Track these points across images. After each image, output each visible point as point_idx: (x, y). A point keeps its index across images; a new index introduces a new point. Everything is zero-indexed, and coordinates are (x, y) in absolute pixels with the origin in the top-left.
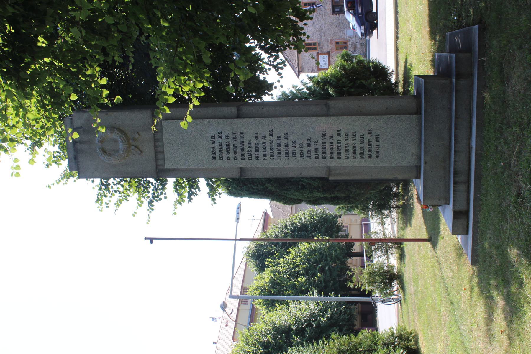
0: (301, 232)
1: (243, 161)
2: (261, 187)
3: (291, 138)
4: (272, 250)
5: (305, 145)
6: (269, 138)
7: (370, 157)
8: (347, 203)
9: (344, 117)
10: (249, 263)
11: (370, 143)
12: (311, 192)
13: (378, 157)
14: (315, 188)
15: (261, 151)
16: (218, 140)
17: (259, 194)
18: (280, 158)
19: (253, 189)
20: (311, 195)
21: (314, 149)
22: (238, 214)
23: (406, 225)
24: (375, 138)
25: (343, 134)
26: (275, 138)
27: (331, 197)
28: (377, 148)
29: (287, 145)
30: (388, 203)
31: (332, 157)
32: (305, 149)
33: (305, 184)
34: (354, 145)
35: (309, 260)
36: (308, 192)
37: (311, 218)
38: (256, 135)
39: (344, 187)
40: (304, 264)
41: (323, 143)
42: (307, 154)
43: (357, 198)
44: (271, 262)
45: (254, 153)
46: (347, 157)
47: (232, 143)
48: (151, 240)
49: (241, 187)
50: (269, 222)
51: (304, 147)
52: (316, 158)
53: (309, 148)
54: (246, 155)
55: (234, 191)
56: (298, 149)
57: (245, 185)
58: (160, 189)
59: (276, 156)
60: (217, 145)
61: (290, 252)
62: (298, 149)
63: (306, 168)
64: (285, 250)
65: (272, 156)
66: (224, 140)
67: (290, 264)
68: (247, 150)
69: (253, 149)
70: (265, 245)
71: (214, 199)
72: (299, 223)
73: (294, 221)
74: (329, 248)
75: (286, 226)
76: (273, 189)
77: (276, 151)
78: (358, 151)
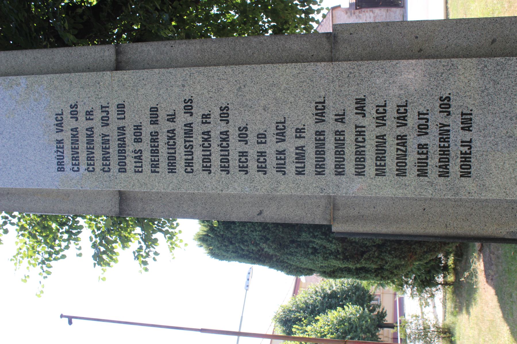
0: (331, 301)
1: (123, 175)
2: (254, 248)
3: (237, 120)
4: (300, 316)
5: (271, 139)
6: (182, 119)
7: (444, 173)
8: (379, 278)
9: (374, 62)
10: (277, 328)
11: (444, 133)
12: (326, 259)
13: (466, 173)
14: (331, 253)
15: (163, 151)
16: (69, 123)
17: (250, 258)
18: (207, 169)
19: (243, 250)
20: (325, 264)
21: (293, 149)
22: (248, 280)
23: (461, 310)
24: (459, 120)
25: (370, 110)
26: (196, 120)
27: (357, 269)
28: (465, 149)
29: (225, 136)
30: (434, 277)
31: (340, 171)
32: (271, 147)
33: (317, 247)
34: (402, 140)
35: (337, 330)
36: (321, 258)
37: (342, 285)
38: (154, 111)
39: (376, 254)
40: (332, 334)
41: (319, 133)
42: (275, 162)
43: (395, 271)
44: (298, 329)
45: (147, 156)
46: (380, 172)
47: (99, 130)
48: (70, 319)
49: (226, 246)
50: (300, 286)
51: (269, 144)
52: (299, 173)
53: (281, 146)
54: (130, 162)
55: (217, 251)
56: (253, 149)
57: (231, 243)
58: (64, 241)
59: (198, 165)
60: (66, 136)
61: (318, 320)
62: (253, 149)
63: (273, 199)
64: (314, 317)
65: (189, 163)
66: (82, 124)
67: (318, 333)
68: (131, 148)
69: (145, 146)
70: (293, 311)
71: (145, 263)
72: (330, 289)
73: (325, 287)
74: (359, 318)
75: (316, 292)
76: (271, 252)
77: (198, 153)
78: (412, 158)
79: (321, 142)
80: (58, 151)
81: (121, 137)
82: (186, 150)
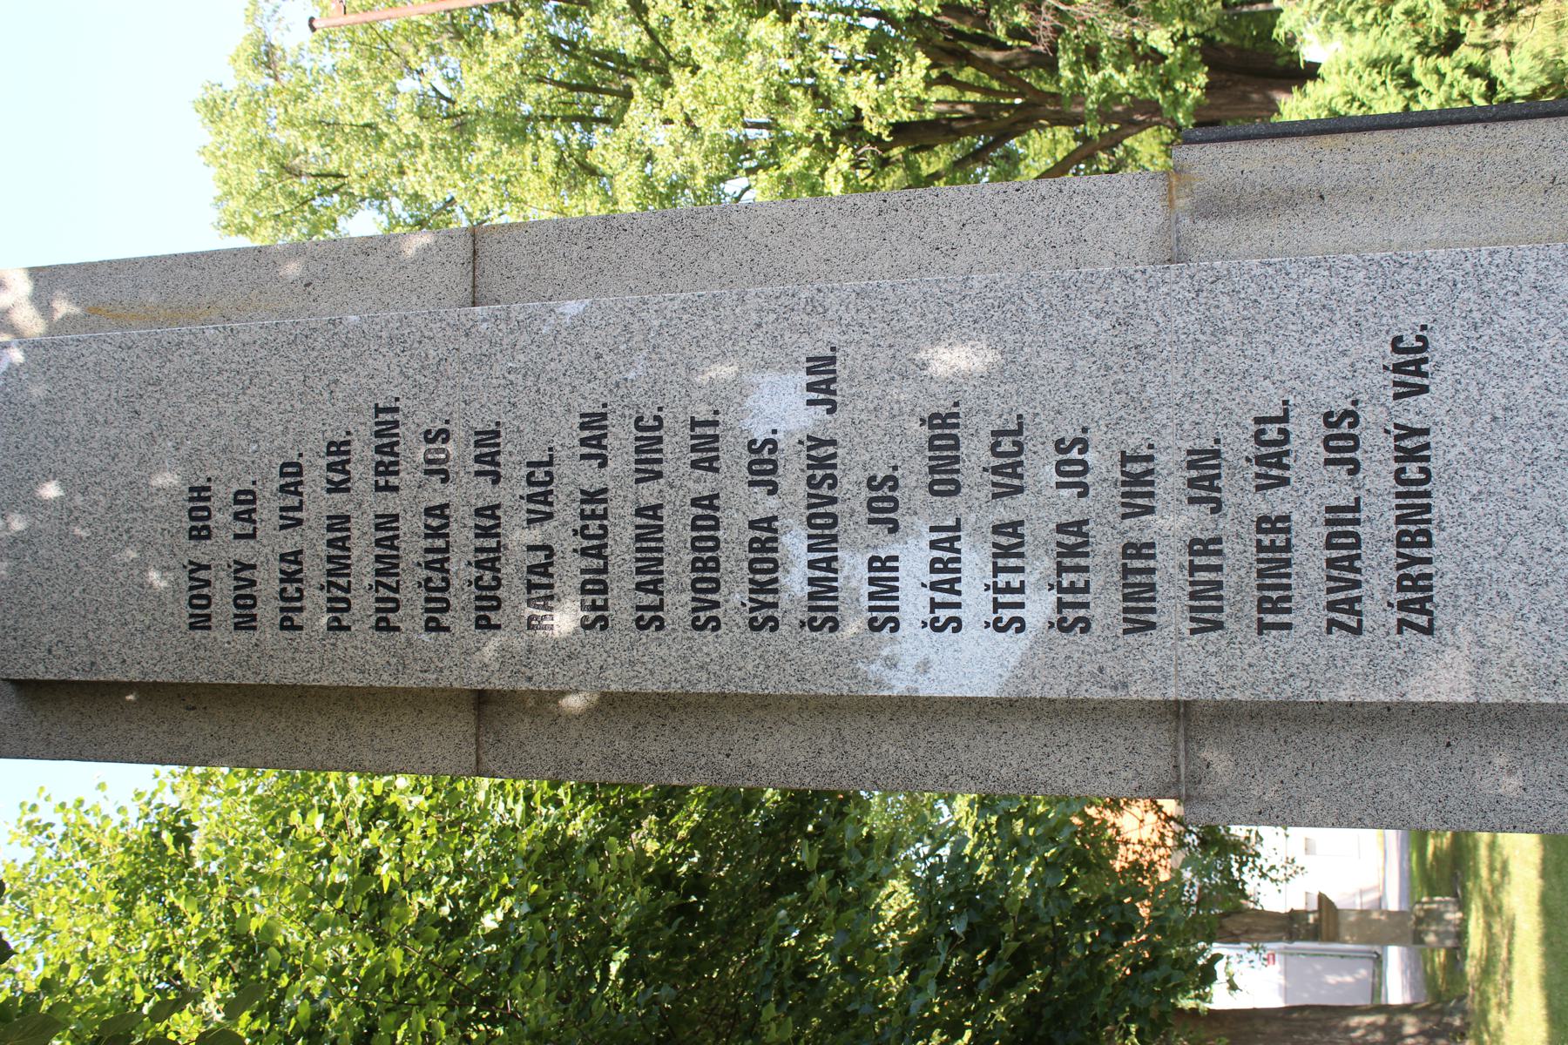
79: (1277, 555)
80: (330, 584)
81: (1341, 596)
82: (894, 614)
